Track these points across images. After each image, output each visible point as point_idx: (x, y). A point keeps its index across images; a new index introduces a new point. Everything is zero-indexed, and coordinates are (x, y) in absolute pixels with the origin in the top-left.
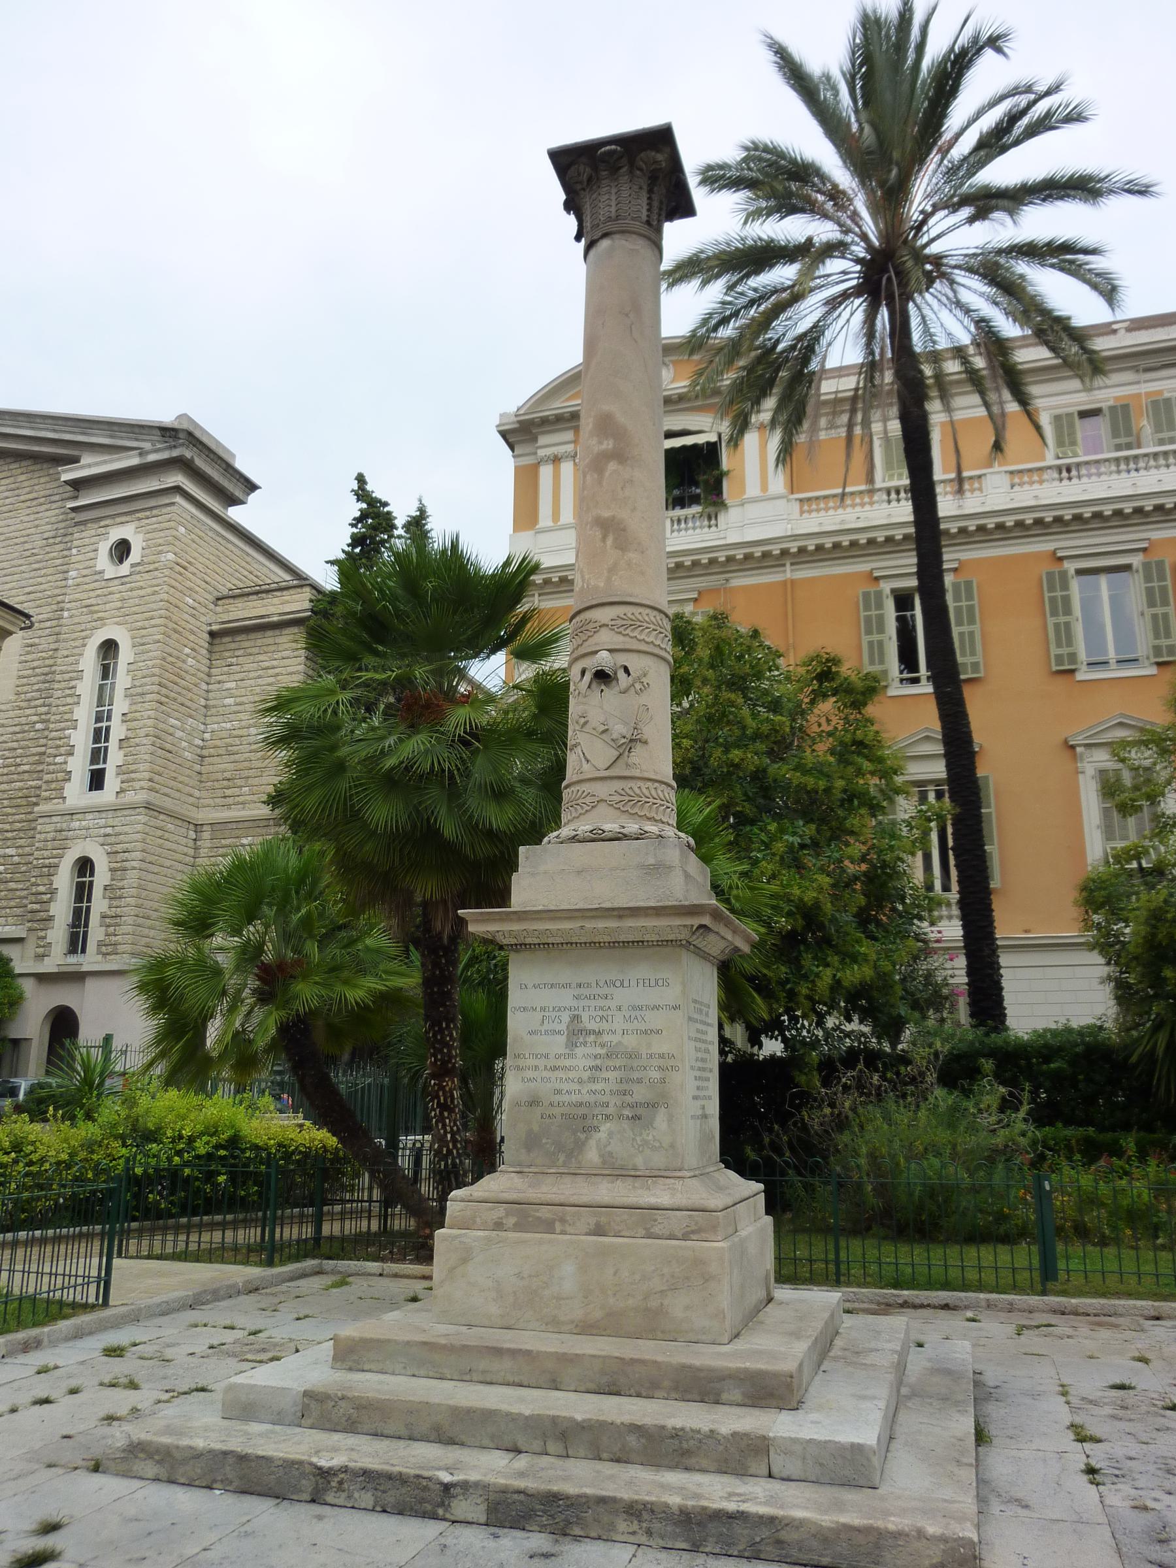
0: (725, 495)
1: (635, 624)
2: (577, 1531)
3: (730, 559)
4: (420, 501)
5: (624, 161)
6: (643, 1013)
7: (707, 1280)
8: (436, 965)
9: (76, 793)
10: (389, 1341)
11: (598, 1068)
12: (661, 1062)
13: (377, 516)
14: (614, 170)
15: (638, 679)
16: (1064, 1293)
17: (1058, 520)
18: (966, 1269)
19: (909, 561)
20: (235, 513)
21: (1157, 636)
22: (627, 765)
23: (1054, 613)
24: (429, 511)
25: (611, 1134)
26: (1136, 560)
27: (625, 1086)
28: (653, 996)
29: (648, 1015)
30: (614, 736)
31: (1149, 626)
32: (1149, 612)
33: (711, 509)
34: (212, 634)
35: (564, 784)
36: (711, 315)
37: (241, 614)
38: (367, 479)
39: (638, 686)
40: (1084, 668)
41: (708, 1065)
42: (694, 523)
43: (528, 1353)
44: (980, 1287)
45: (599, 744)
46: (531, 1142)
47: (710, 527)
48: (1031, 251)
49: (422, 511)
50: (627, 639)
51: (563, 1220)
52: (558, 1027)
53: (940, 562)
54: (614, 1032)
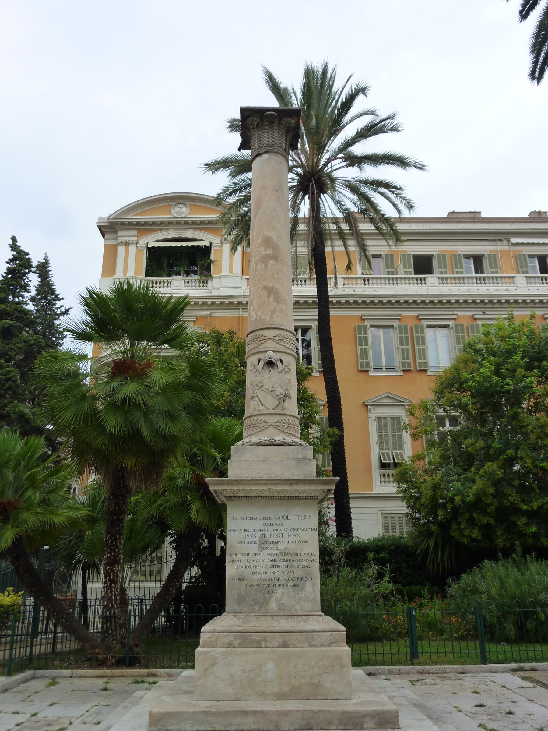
0: (212, 272)
1: (284, 339)
3: (213, 303)
4: (46, 255)
5: (276, 120)
6: (298, 533)
7: (342, 667)
8: (117, 504)
10: (182, 712)
11: (275, 561)
12: (308, 557)
13: (22, 259)
14: (271, 123)
15: (287, 367)
16: (419, 664)
17: (364, 302)
18: (369, 655)
19: (314, 313)
21: (403, 359)
22: (283, 408)
23: (360, 344)
24: (50, 261)
25: (283, 594)
26: (396, 324)
27: (290, 570)
28: (304, 524)
29: (301, 534)
30: (277, 394)
31: (401, 354)
32: (400, 347)
33: (204, 278)
35: (244, 417)
36: (228, 188)
38: (18, 239)
39: (287, 370)
40: (372, 370)
41: (313, 557)
42: (192, 284)
43: (262, 712)
44: (383, 664)
45: (269, 397)
46: (240, 600)
47: (203, 286)
48: (377, 184)
49: (47, 261)
50: (281, 346)
51: (265, 640)
52: (253, 539)
54: (284, 542)
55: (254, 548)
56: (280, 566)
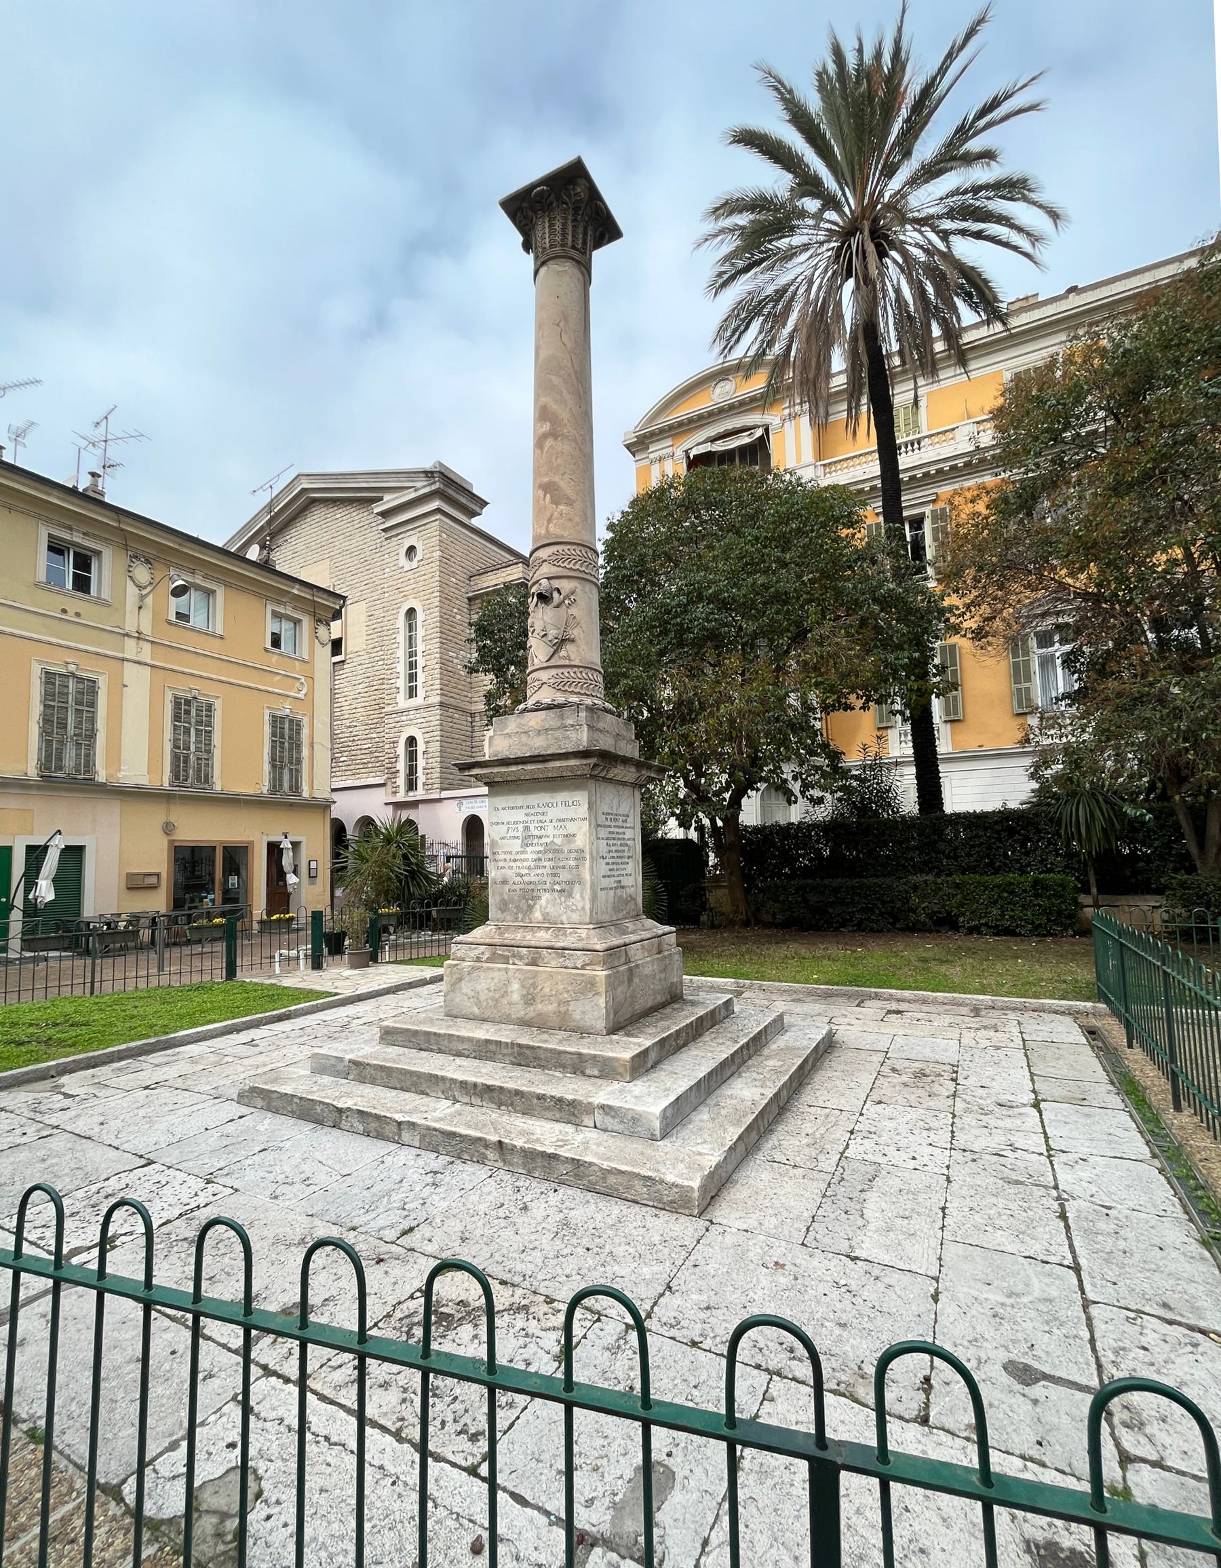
2: (466, 1156)
9: (402, 701)
20: (475, 522)
28: (571, 813)
34: (469, 599)
37: (485, 585)
53: (900, 502)
55: (516, 845)
56: (544, 867)
